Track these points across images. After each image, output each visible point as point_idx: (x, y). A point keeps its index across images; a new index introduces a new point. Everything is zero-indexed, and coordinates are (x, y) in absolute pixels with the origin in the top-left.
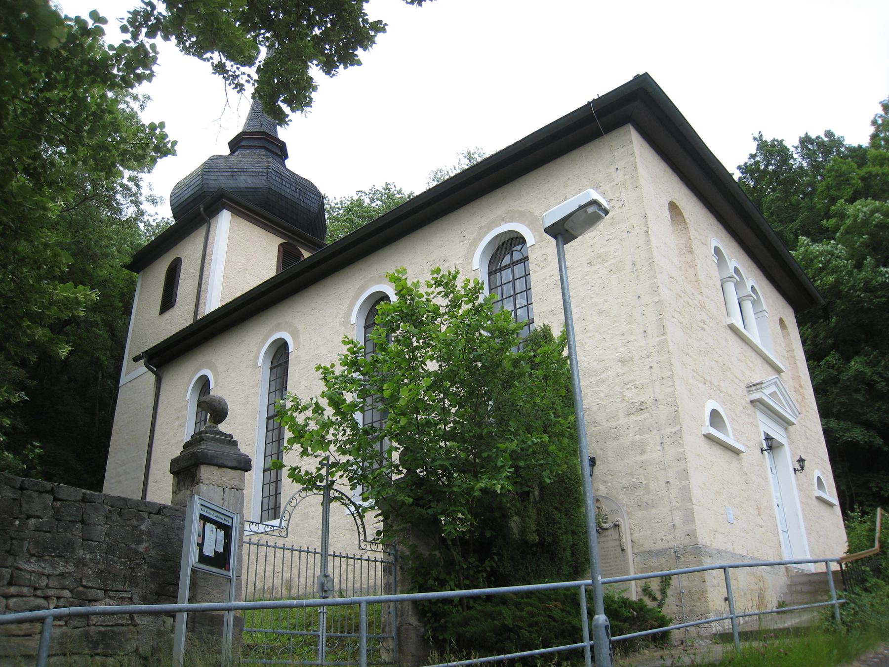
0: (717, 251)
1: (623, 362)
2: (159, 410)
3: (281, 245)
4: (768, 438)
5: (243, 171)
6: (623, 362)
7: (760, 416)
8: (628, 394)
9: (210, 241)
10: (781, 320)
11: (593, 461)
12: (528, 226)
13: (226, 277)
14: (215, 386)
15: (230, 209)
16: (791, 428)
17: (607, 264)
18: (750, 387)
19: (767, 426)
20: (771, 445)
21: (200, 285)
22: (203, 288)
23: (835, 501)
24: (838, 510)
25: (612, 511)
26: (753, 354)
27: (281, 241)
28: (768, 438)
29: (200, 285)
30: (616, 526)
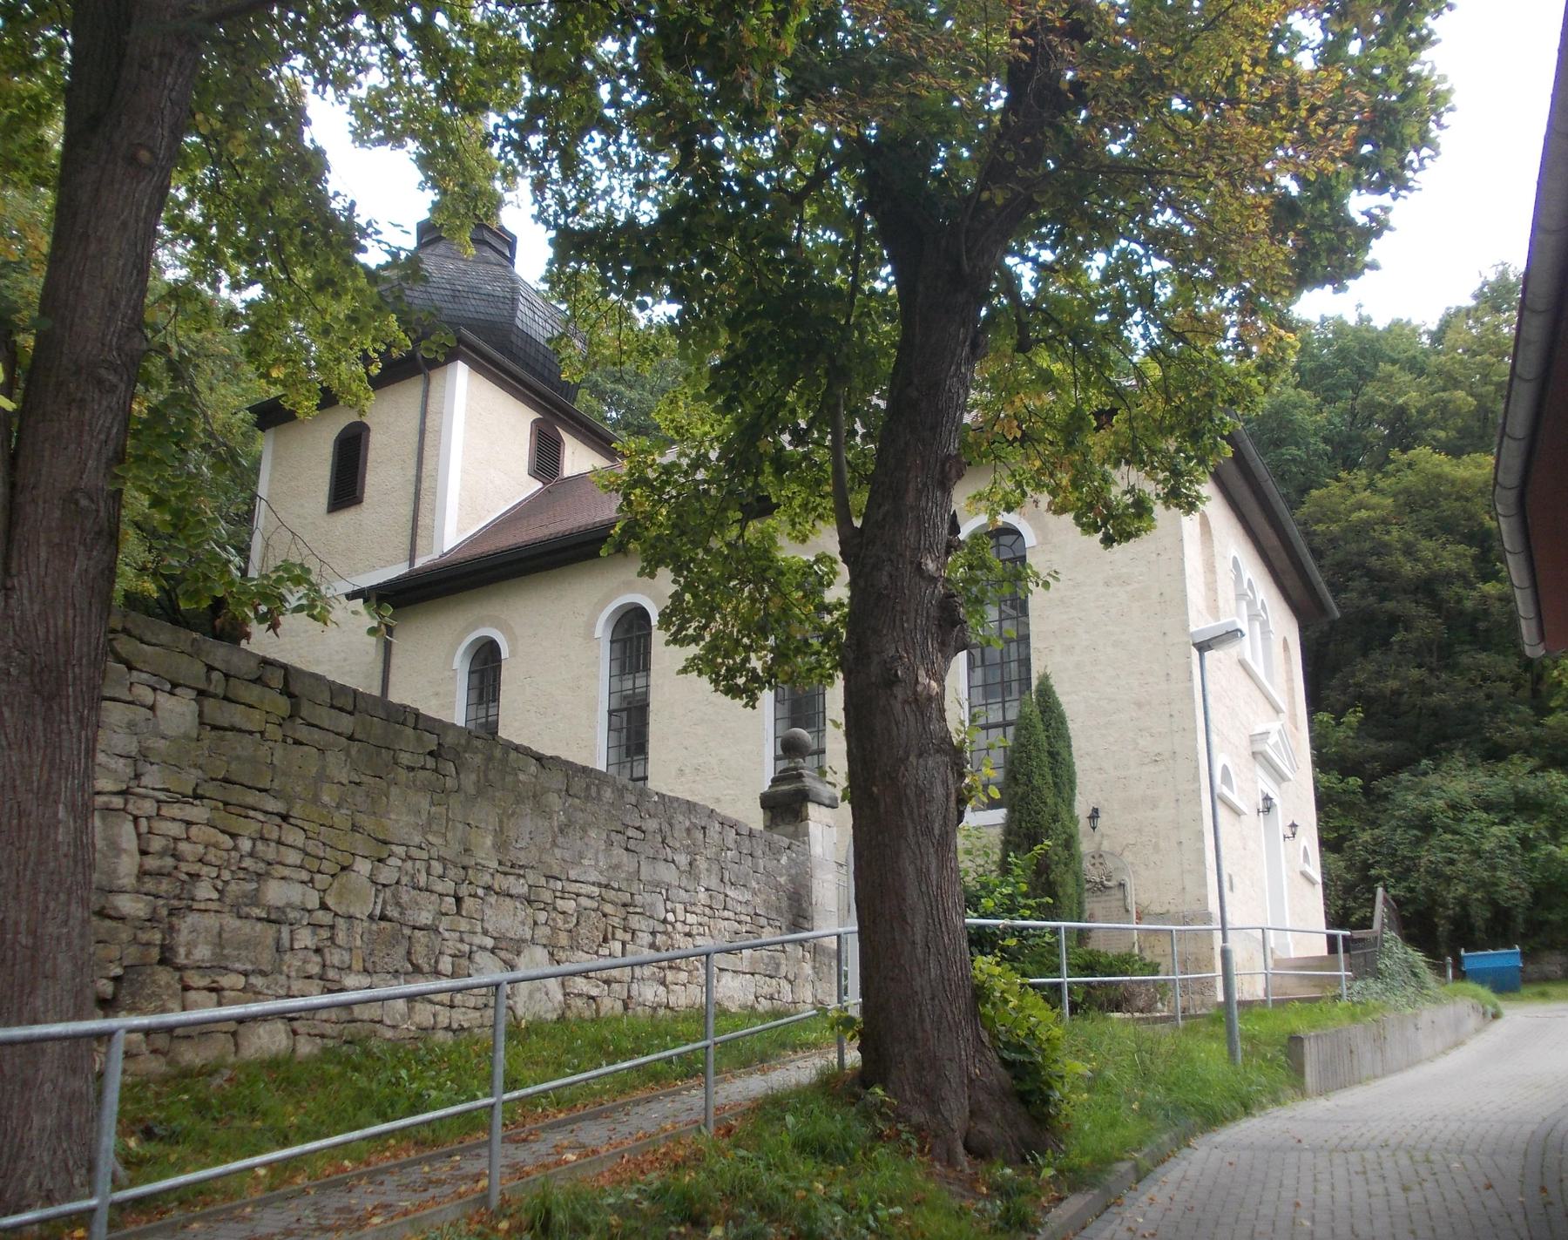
0: (1235, 561)
1: (1139, 705)
2: (393, 678)
3: (535, 421)
4: (1267, 799)
5: (474, 291)
6: (1139, 705)
7: (1260, 772)
8: (1142, 742)
9: (432, 408)
10: (1285, 640)
11: (1095, 815)
12: (1029, 521)
13: (464, 471)
14: (513, 653)
15: (468, 361)
16: (1284, 785)
17: (1129, 588)
18: (1253, 739)
19: (1267, 785)
20: (1268, 806)
21: (419, 479)
22: (425, 485)
23: (1318, 878)
24: (1319, 889)
25: (1116, 869)
26: (1257, 693)
27: (535, 415)
28: (1267, 799)
29: (419, 479)
30: (1122, 885)
